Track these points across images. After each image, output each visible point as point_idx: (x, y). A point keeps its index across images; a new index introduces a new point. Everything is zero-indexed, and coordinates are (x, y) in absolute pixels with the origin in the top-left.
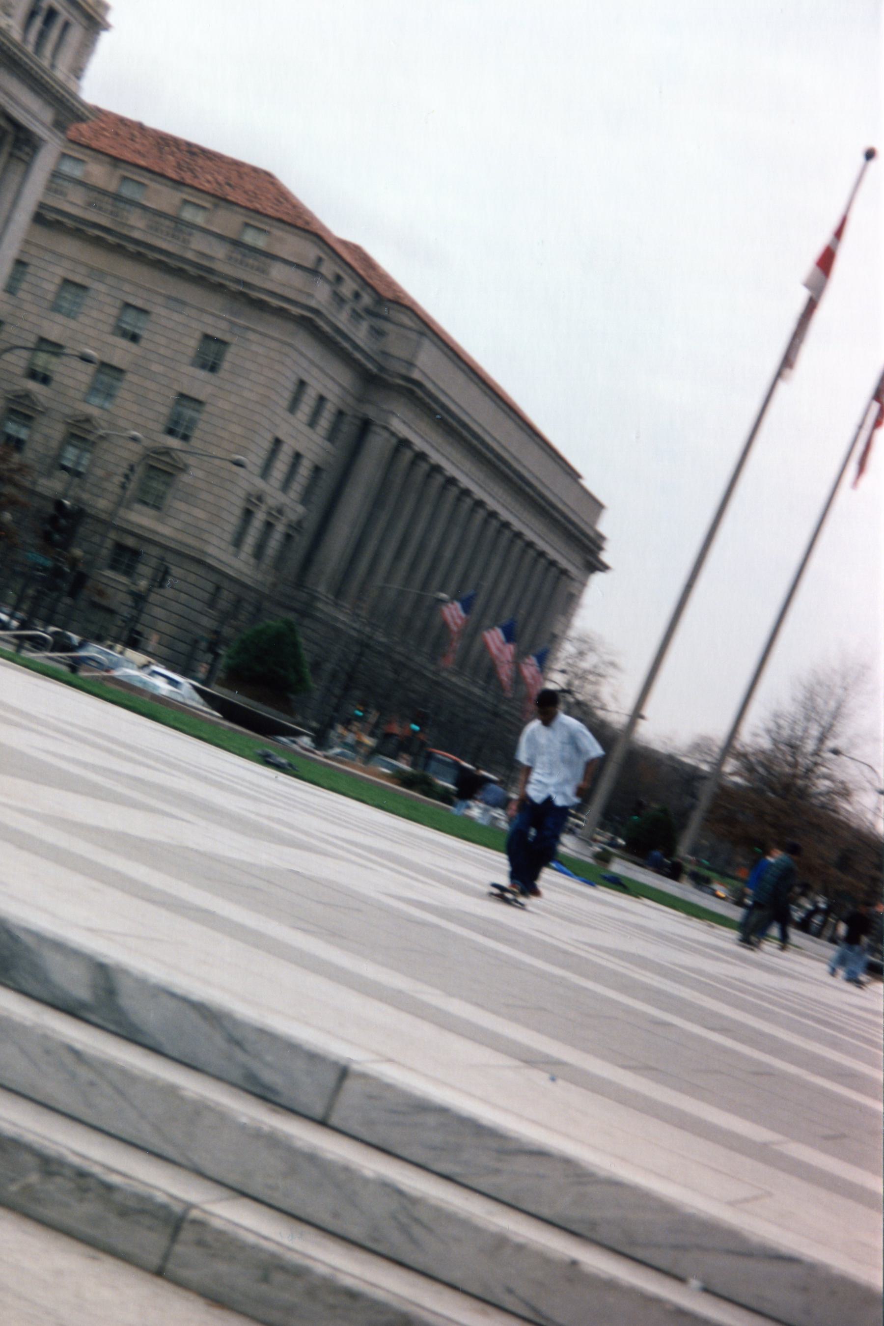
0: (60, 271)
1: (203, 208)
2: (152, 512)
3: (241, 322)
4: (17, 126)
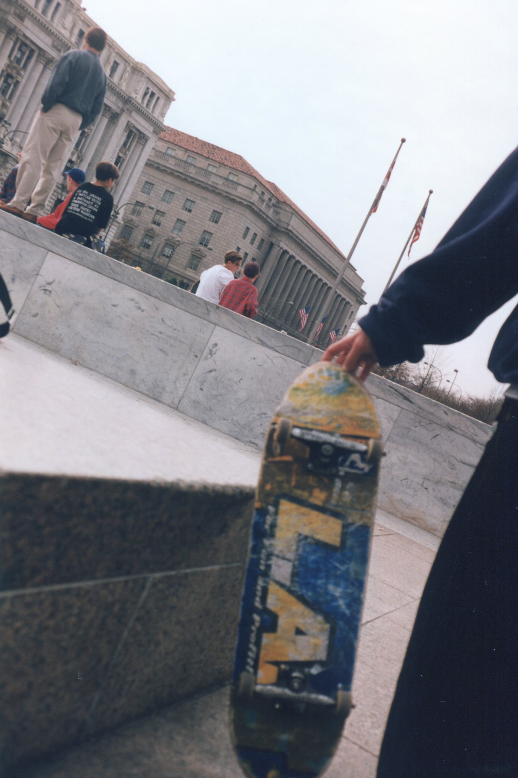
0: (165, 188)
1: (216, 167)
2: (193, 271)
3: (227, 206)
4: (140, 132)
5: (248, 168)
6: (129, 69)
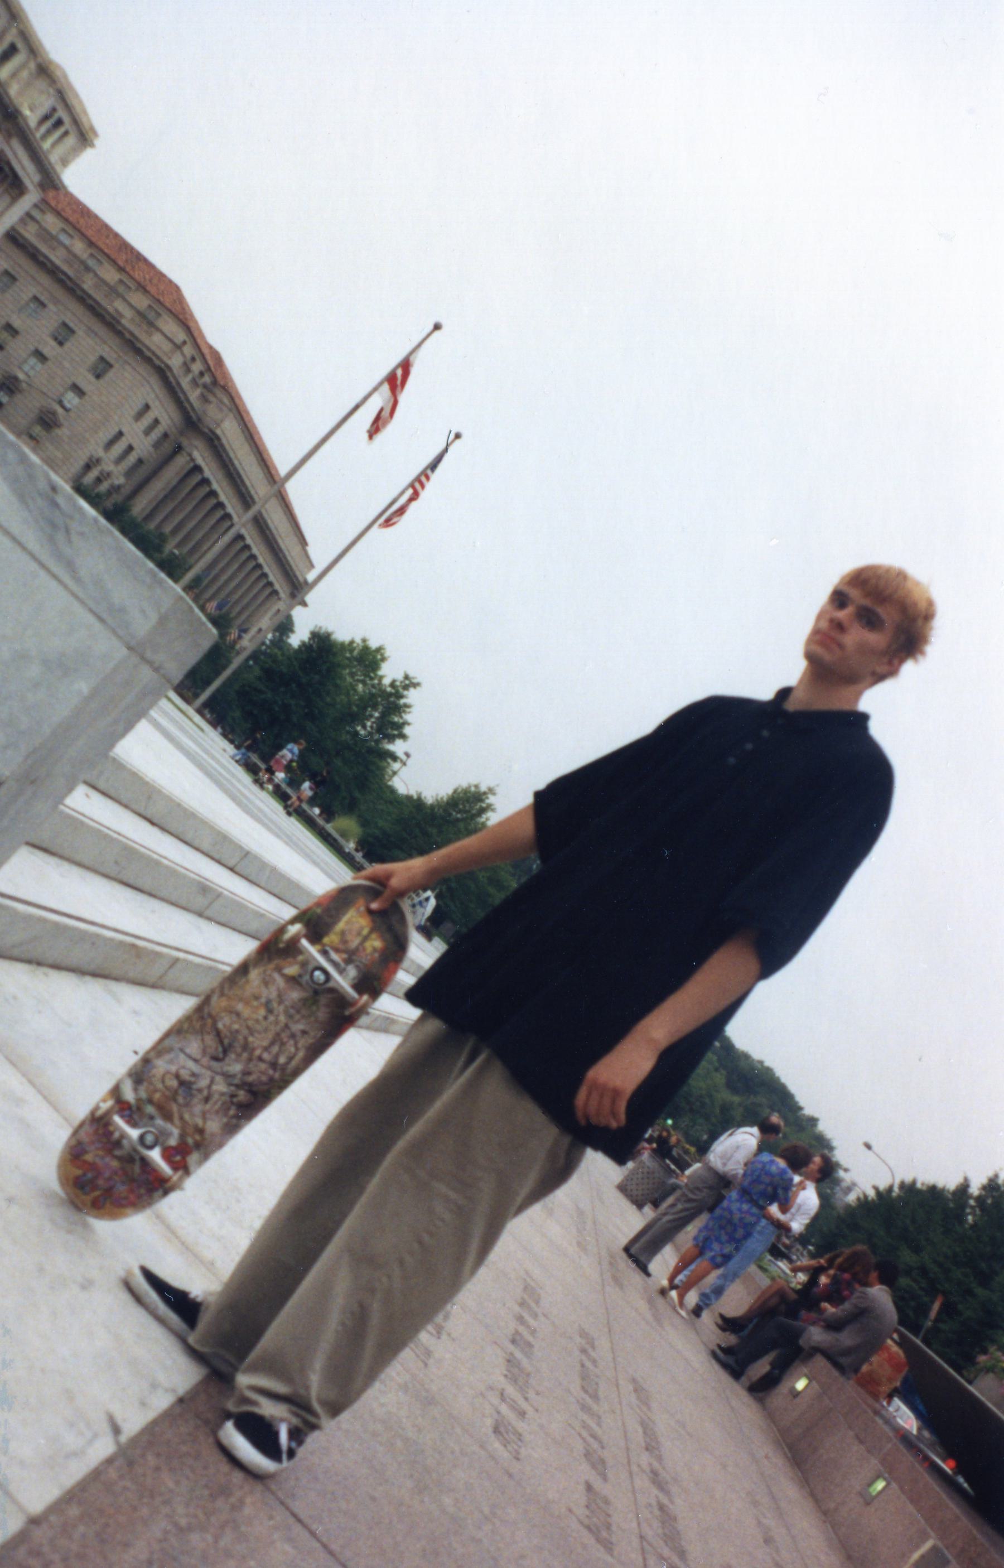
5: (183, 309)
6: (32, 65)
